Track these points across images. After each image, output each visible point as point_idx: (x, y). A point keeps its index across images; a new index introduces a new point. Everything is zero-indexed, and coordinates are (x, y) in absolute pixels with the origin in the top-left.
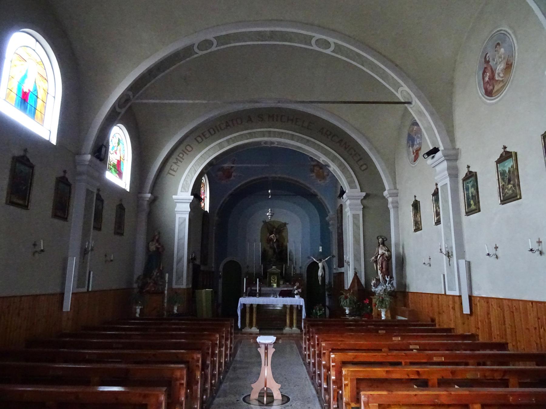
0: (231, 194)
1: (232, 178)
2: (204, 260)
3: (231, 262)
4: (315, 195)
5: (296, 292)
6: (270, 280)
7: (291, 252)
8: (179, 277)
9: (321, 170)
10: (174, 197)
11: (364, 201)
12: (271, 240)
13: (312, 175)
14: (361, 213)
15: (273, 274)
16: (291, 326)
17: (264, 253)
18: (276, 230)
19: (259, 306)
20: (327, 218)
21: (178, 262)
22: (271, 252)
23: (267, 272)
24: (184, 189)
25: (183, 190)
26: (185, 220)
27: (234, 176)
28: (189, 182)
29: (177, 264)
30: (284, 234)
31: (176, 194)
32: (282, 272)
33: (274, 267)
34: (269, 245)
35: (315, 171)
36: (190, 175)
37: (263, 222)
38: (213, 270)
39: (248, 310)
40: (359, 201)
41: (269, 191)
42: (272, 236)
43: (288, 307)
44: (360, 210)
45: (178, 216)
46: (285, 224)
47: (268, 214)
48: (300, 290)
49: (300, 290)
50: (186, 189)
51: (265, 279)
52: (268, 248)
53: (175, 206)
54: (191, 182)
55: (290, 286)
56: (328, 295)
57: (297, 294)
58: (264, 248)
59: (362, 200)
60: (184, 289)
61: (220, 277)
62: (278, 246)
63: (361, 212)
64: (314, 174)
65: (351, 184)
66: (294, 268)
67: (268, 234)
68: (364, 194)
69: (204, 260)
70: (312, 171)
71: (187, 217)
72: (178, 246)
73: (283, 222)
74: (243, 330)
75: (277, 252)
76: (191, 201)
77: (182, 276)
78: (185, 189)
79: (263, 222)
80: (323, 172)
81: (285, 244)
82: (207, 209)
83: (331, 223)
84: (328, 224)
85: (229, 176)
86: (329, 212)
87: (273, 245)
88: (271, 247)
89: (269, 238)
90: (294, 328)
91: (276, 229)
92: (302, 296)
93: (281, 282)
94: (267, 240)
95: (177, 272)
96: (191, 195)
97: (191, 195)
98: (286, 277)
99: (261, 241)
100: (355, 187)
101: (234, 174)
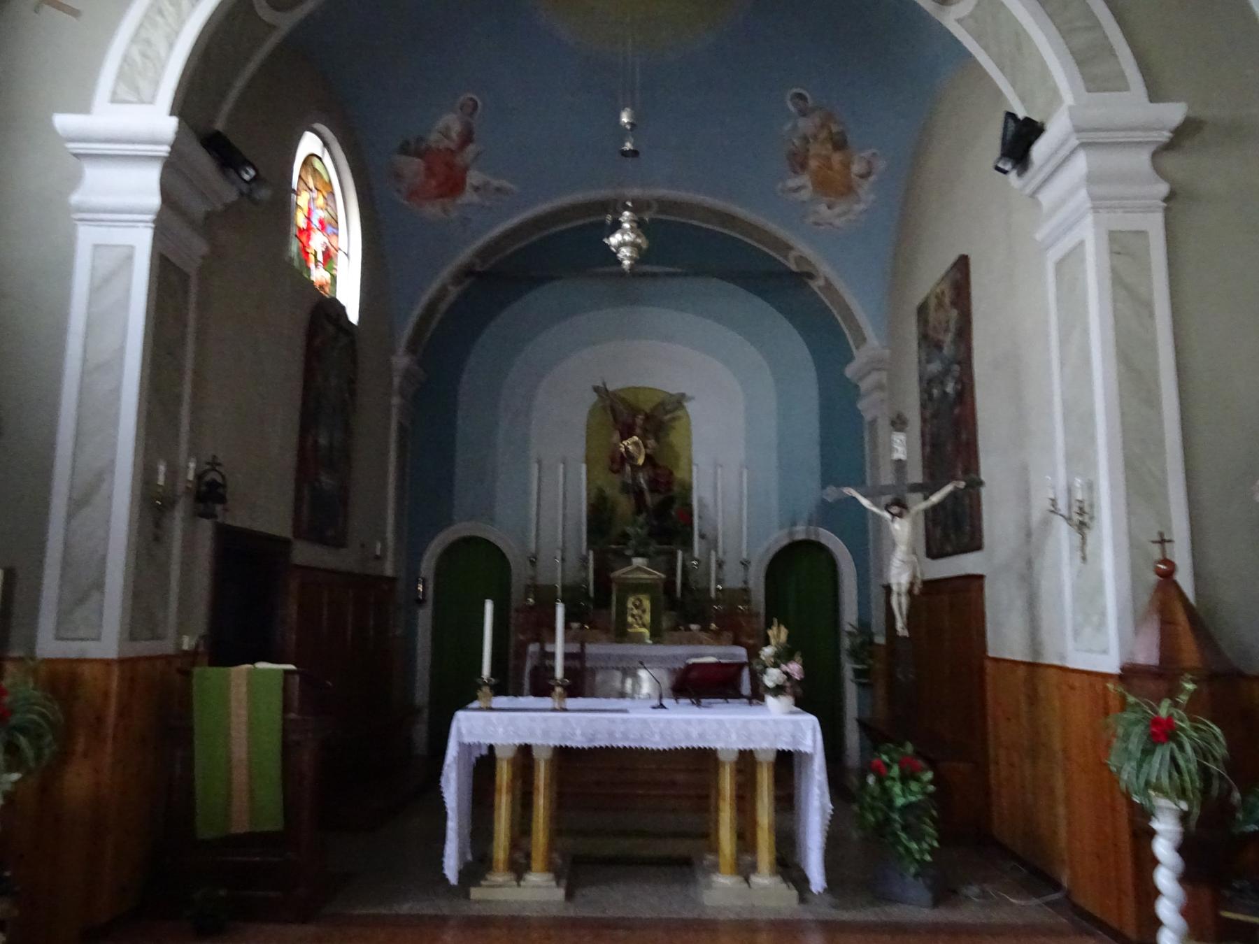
0: (467, 272)
1: (469, 197)
2: (323, 512)
3: (470, 543)
4: (802, 278)
5: (772, 677)
6: (622, 611)
7: (702, 505)
8: (84, 589)
9: (837, 158)
10: (64, 122)
11: (1170, 161)
12: (628, 457)
13: (793, 183)
14: (1154, 225)
15: (638, 588)
16: (745, 870)
17: (600, 516)
18: (640, 427)
19: (565, 756)
20: (850, 371)
21: (78, 504)
22: (625, 505)
23: (610, 581)
24: (132, 88)
25: (123, 91)
26: (129, 258)
27: (477, 189)
28: (162, 48)
29: (70, 516)
30: (675, 438)
31: (84, 107)
32: (669, 584)
33: (638, 561)
34: (617, 479)
35: (813, 164)
36: (169, 9)
37: (596, 389)
38: (389, 570)
39: (504, 774)
40: (1142, 160)
41: (625, 119)
42: (629, 444)
43: (728, 759)
44: (1148, 209)
45: (87, 237)
46: (679, 401)
47: (615, 240)
48: (795, 668)
49: (795, 668)
50: (143, 85)
51: (596, 607)
52: (613, 491)
53: (75, 180)
54: (171, 46)
55: (704, 636)
56: (858, 674)
57: (778, 691)
58: (601, 491)
59: (1155, 155)
60: (107, 663)
61: (421, 603)
62: (654, 484)
63: (1158, 218)
64: (804, 179)
65: (1092, 65)
66: (720, 565)
67: (616, 437)
68: (1174, 113)
69: (323, 512)
70: (798, 162)
71: (142, 240)
72: (80, 404)
73: (674, 392)
74: (475, 893)
75: (646, 504)
76: (164, 150)
77: (99, 586)
78: (137, 90)
79: (596, 389)
80: (847, 165)
81: (679, 475)
82: (349, 296)
83: (864, 385)
84: (852, 391)
85: (453, 184)
86: (861, 339)
87: (634, 478)
88: (625, 488)
89: (616, 446)
90: (765, 879)
91: (648, 418)
92: (804, 703)
93: (665, 623)
94: (613, 460)
95: (66, 563)
96: (172, 114)
97: (172, 114)
98: (684, 607)
99: (588, 461)
100: (1120, 83)
101: (474, 177)
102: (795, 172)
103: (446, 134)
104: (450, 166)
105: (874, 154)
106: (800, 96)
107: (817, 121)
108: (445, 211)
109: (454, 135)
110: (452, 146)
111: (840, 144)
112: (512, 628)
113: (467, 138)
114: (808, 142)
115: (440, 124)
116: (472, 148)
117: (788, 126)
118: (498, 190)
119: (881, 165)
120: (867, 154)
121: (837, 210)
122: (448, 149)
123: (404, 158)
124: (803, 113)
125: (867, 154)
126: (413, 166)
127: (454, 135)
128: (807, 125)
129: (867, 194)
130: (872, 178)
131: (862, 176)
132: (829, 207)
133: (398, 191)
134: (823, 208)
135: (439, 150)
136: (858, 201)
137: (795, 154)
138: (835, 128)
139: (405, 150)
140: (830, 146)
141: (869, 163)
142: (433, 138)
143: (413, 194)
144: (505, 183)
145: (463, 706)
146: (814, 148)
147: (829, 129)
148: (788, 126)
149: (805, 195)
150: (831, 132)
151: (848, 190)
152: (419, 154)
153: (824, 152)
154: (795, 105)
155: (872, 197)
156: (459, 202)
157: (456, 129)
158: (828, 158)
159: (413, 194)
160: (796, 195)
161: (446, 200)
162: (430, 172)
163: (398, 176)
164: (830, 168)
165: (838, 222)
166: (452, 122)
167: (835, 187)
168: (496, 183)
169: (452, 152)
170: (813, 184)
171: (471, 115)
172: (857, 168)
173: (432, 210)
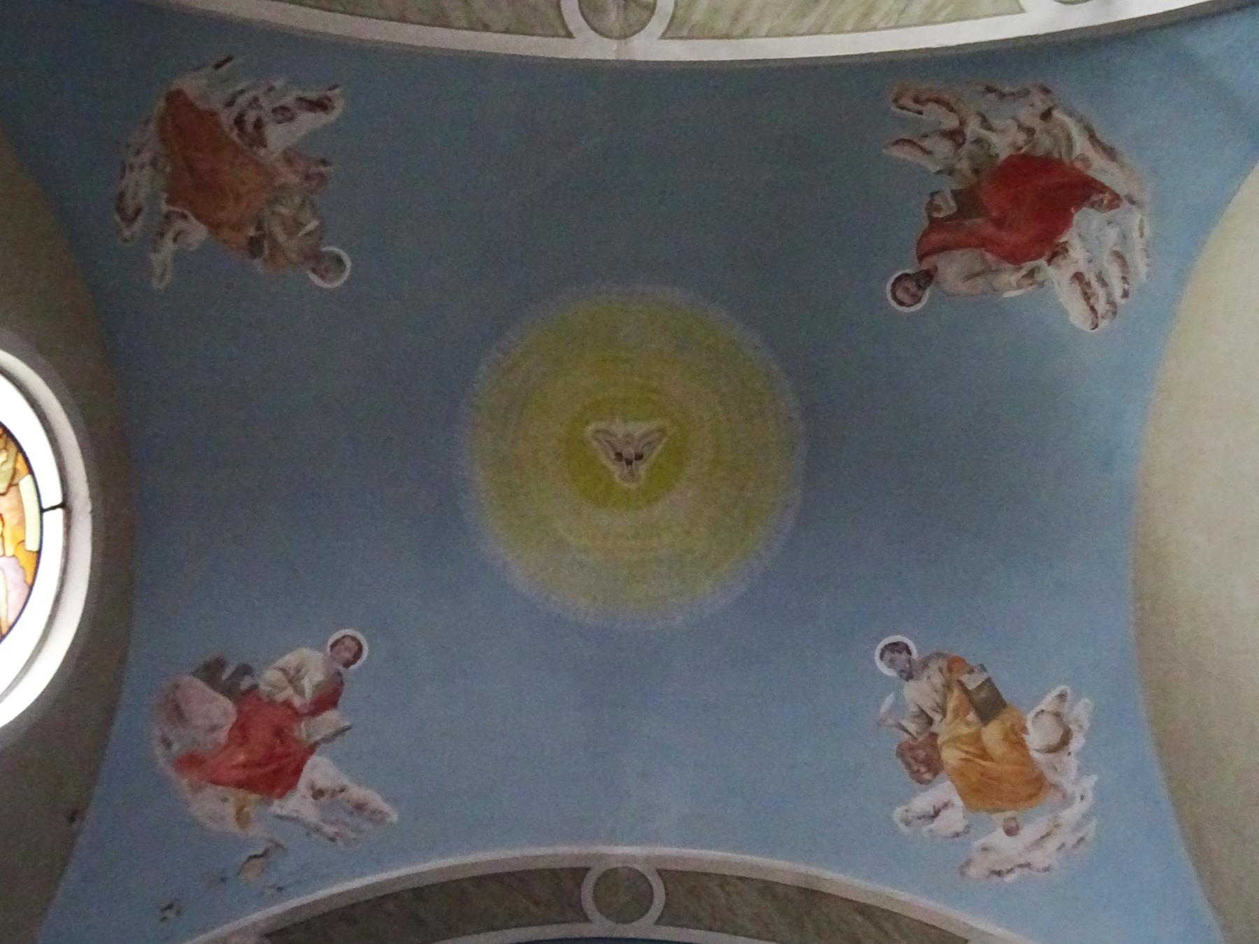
1: (298, 803)
9: (992, 734)
13: (924, 801)
27: (318, 794)
35: (951, 756)
64: (944, 790)
70: (923, 760)
80: (1015, 739)
85: (275, 771)
101: (320, 770)
102: (920, 782)
103: (294, 678)
104: (279, 733)
105: (1062, 697)
106: (894, 647)
107: (938, 680)
108: (241, 817)
109: (308, 685)
110: (297, 702)
111: (989, 705)
112: (1008, 814)
113: (327, 699)
114: (930, 721)
115: (290, 659)
116: (331, 717)
117: (889, 700)
118: (360, 807)
119: (1081, 711)
120: (1048, 702)
121: (1030, 832)
122: (287, 704)
123: (199, 684)
124: (908, 675)
125: (1048, 702)
126: (214, 712)
127: (308, 685)
128: (919, 693)
129: (1076, 780)
130: (1077, 743)
131: (1053, 750)
132: (1011, 832)
133: (167, 743)
134: (998, 837)
135: (272, 702)
136: (1067, 800)
137: (912, 748)
138: (972, 682)
139: (211, 672)
140: (971, 716)
141: (1057, 715)
142: (269, 678)
143: (191, 762)
144: (376, 800)
145: (1079, 207)
146: (943, 728)
147: (961, 684)
148: (889, 700)
149: (955, 818)
150: (965, 691)
151: (1035, 786)
152: (229, 691)
153: (964, 730)
154: (891, 664)
155: (1090, 782)
156: (277, 807)
157: (314, 677)
158: (977, 739)
159: (191, 762)
160: (935, 824)
161: (253, 797)
162: (242, 730)
163: (177, 713)
164: (984, 754)
165: (1040, 858)
166: (313, 666)
167: (1009, 787)
168: (357, 792)
169: (297, 715)
170: (963, 796)
171: (347, 664)
172: (1036, 738)
173: (214, 807)
